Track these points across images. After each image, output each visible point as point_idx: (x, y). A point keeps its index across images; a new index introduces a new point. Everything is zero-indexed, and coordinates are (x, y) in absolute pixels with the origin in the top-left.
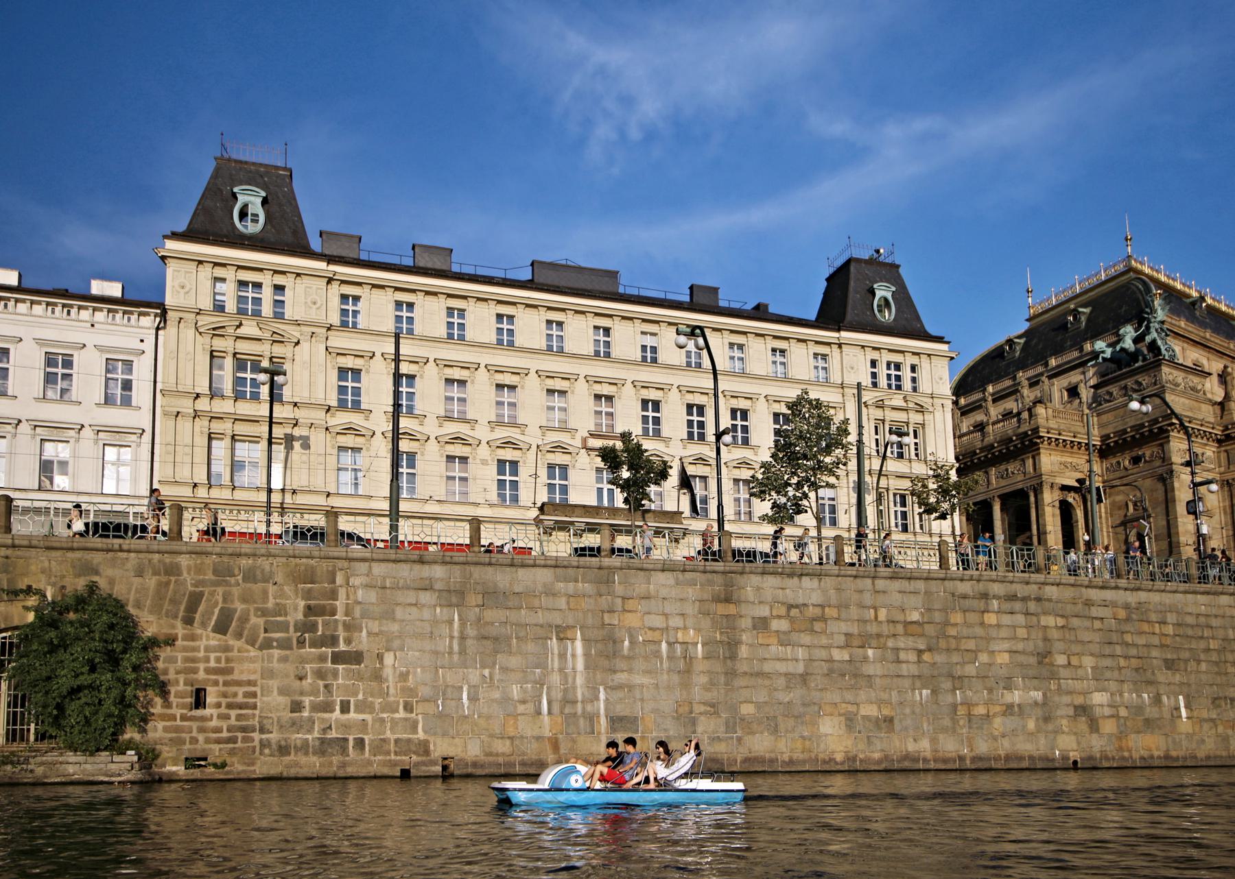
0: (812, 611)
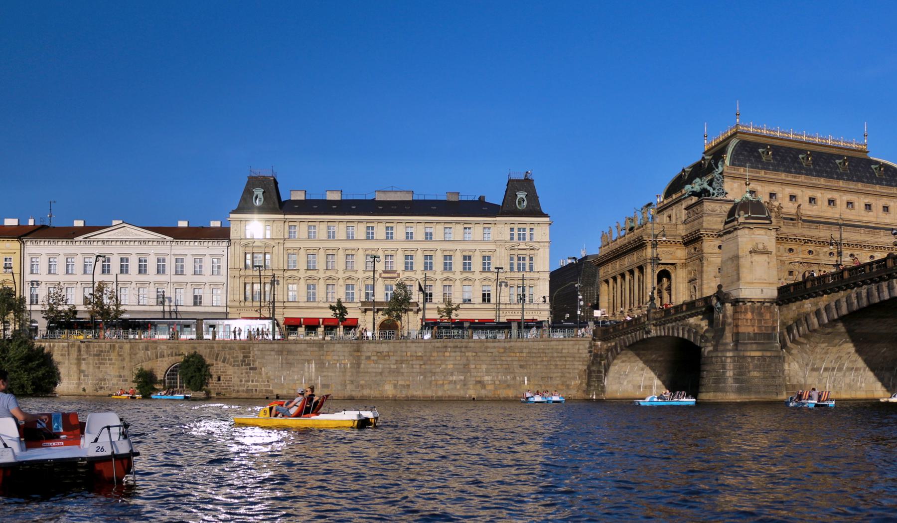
0: (385, 354)
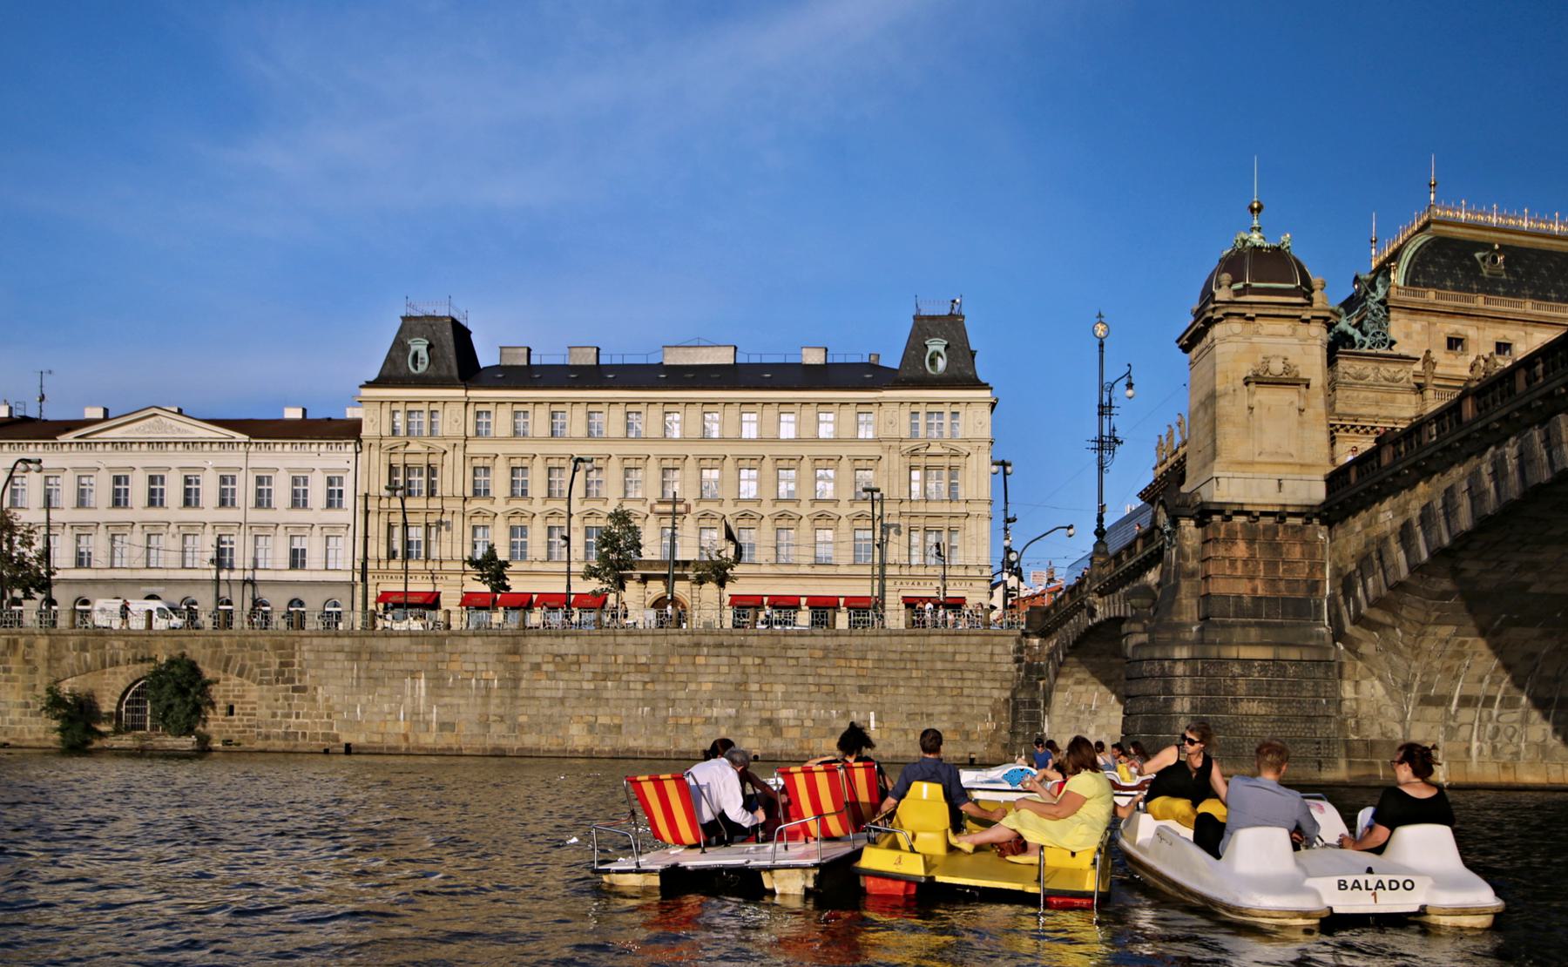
0: (570, 659)
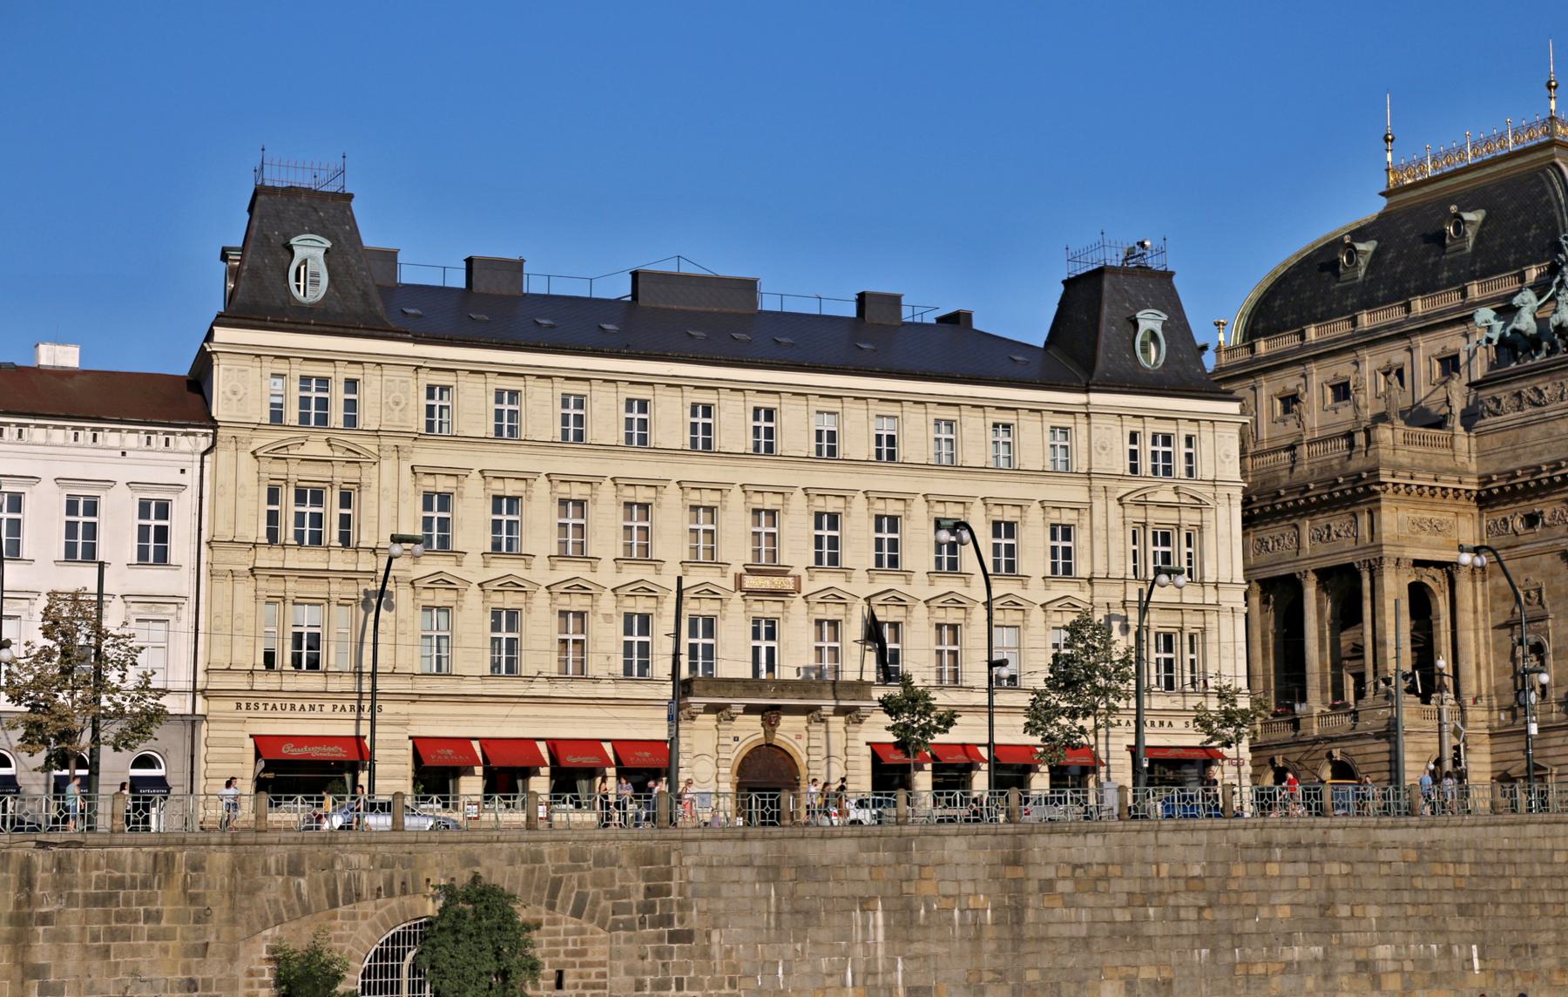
0: (1096, 870)
